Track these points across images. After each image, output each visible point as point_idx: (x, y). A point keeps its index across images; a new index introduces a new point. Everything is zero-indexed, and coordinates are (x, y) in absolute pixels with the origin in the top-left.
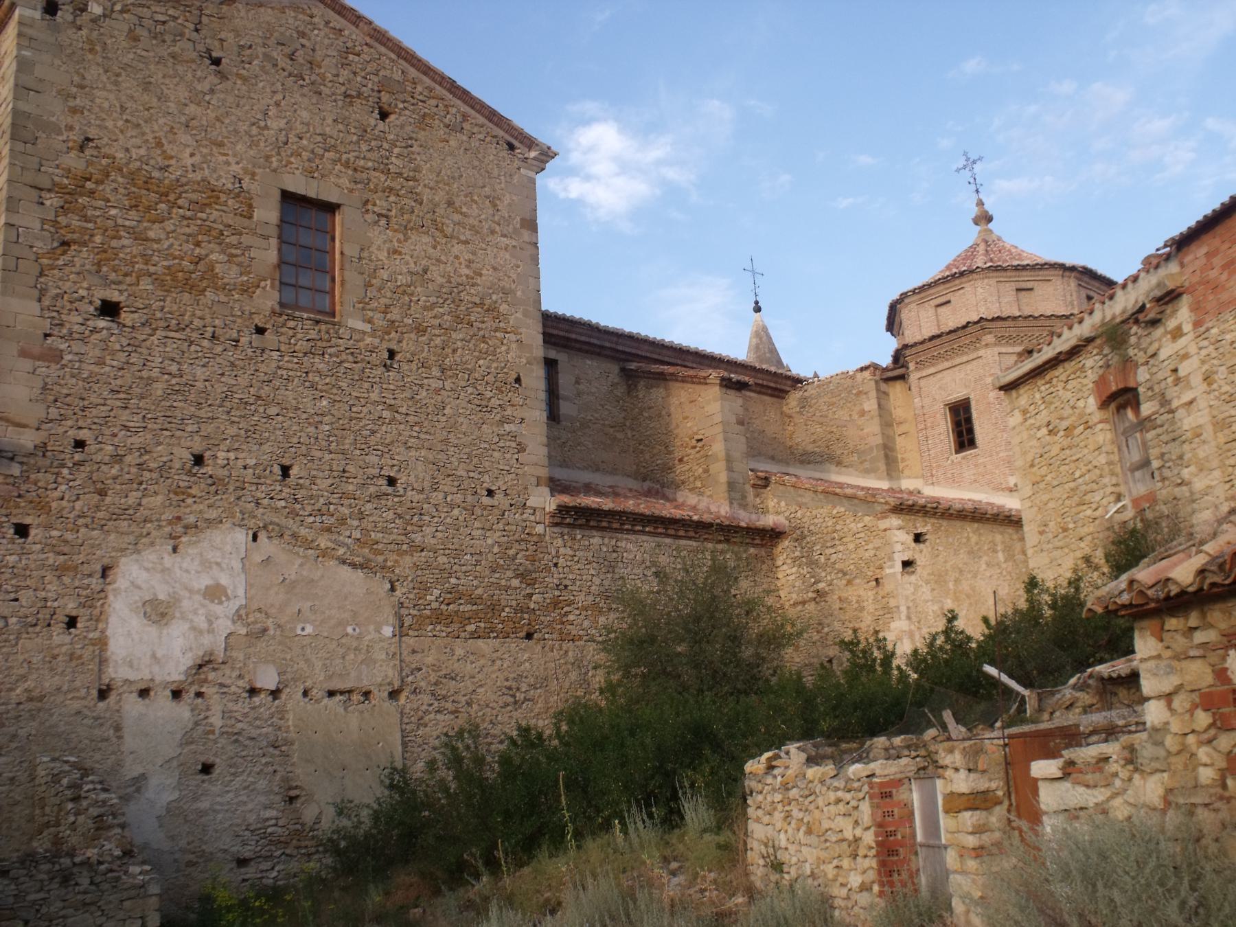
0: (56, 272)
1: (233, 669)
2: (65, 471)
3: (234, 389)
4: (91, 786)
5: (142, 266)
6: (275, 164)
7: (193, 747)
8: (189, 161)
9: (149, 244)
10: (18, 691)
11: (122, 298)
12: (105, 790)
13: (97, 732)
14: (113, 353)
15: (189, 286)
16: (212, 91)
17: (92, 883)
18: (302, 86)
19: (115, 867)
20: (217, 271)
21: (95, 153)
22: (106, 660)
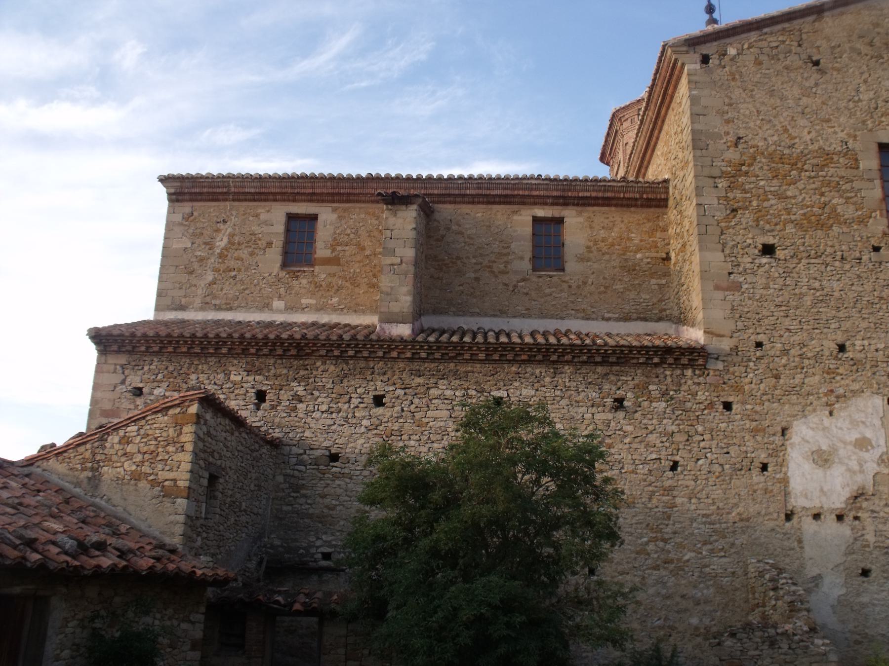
0: (731, 230)
1: (880, 499)
2: (751, 364)
3: (863, 294)
4: (784, 581)
5: (786, 217)
6: (870, 126)
7: (854, 556)
8: (808, 137)
9: (788, 200)
10: (733, 514)
11: (775, 241)
12: (794, 584)
13: (786, 543)
14: (774, 280)
15: (821, 225)
16: (816, 85)
17: (790, 648)
18: (882, 63)
19: (805, 639)
20: (839, 211)
21: (745, 146)
22: (789, 493)
